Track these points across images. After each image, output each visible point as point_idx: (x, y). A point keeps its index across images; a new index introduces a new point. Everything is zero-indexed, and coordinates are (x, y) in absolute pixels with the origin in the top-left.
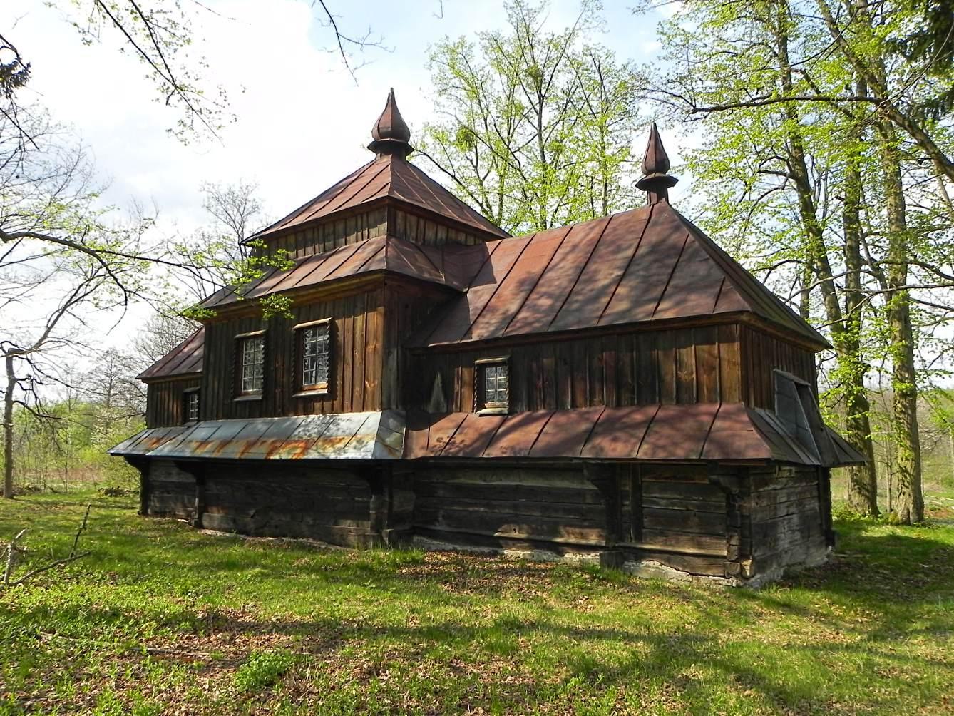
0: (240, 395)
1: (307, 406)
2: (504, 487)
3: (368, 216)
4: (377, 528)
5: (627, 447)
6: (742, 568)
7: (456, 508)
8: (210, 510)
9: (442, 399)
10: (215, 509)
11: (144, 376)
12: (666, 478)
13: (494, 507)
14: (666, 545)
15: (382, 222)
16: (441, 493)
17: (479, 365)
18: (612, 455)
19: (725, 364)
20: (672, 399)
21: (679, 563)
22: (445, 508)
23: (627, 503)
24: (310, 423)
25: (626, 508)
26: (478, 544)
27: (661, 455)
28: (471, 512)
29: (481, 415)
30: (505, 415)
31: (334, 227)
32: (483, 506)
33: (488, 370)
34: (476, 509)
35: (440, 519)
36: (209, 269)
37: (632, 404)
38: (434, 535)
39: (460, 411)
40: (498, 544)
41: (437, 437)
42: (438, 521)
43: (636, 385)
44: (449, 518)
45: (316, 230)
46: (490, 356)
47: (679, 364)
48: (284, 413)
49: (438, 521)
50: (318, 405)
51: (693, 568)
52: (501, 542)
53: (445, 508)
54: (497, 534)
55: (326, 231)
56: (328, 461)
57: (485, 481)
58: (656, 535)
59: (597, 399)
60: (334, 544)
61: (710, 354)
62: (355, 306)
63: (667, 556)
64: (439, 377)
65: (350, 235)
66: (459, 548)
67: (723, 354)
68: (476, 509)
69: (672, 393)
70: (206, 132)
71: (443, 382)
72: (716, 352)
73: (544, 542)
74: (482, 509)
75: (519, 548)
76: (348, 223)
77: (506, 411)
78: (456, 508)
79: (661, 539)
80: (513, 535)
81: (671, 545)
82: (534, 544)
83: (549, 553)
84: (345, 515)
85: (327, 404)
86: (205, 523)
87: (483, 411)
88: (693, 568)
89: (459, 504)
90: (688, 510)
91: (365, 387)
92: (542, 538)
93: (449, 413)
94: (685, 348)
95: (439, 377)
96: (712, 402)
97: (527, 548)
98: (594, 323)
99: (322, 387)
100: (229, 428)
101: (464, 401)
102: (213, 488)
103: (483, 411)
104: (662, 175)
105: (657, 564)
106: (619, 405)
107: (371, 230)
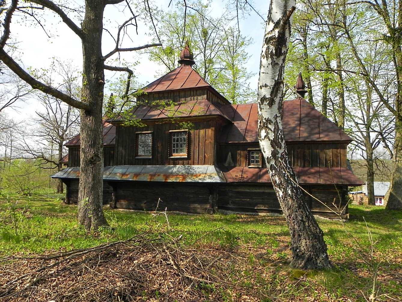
0: (138, 156)
1: (176, 162)
2: (255, 192)
3: (196, 92)
4: (212, 206)
5: (315, 180)
6: (347, 216)
7: (237, 199)
8: (119, 201)
9: (232, 161)
10: (122, 201)
11: (68, 144)
12: (321, 190)
13: (254, 199)
14: (320, 210)
15: (204, 95)
16: (230, 194)
17: (249, 150)
18: (311, 182)
19: (342, 155)
20: (323, 165)
21: (325, 216)
22: (232, 199)
23: (306, 197)
24: (177, 168)
25: (306, 199)
26: (248, 212)
27: (328, 183)
28: (243, 201)
29: (249, 168)
30: (260, 168)
31: (179, 93)
32: (249, 199)
33: (140, 136)
34: (246, 200)
35: (230, 203)
36: (363, 151)
37: (309, 166)
38: (228, 209)
39: (240, 166)
40: (257, 211)
41: (234, 174)
42: (229, 204)
43: (311, 160)
44: (234, 203)
45: (169, 93)
46: (251, 148)
47: (326, 154)
48: (163, 163)
49: (229, 204)
50: (181, 162)
51: (330, 217)
52: (257, 210)
53: (232, 199)
54: (255, 208)
55: (175, 94)
56: (173, 182)
57: (250, 190)
58: (317, 207)
59: (296, 164)
60: (190, 213)
61: (337, 152)
62: (200, 126)
63: (320, 213)
64: (230, 154)
65: (188, 97)
66: (239, 213)
67: (342, 152)
68: (246, 200)
69: (324, 163)
70: (34, 22)
71: (232, 155)
72: (339, 151)
73: (252, 209)
74: (248, 200)
75: (264, 213)
76: (186, 93)
77: (261, 166)
78: (237, 199)
79: (318, 208)
80: (263, 208)
81: (322, 210)
82: (269, 211)
83: (277, 214)
84: (194, 202)
85: (185, 162)
86: (118, 206)
87: (250, 166)
88: (330, 217)
89: (238, 198)
90: (328, 199)
91: (205, 156)
92: (274, 209)
93: (235, 167)
94: (328, 149)
95: (230, 154)
96: (337, 166)
97: (268, 213)
98: (297, 140)
99: (184, 155)
100: (137, 169)
101: (241, 162)
102: (121, 192)
103: (250, 166)
104: (303, 90)
105: (318, 216)
106: (304, 167)
107: (198, 97)
